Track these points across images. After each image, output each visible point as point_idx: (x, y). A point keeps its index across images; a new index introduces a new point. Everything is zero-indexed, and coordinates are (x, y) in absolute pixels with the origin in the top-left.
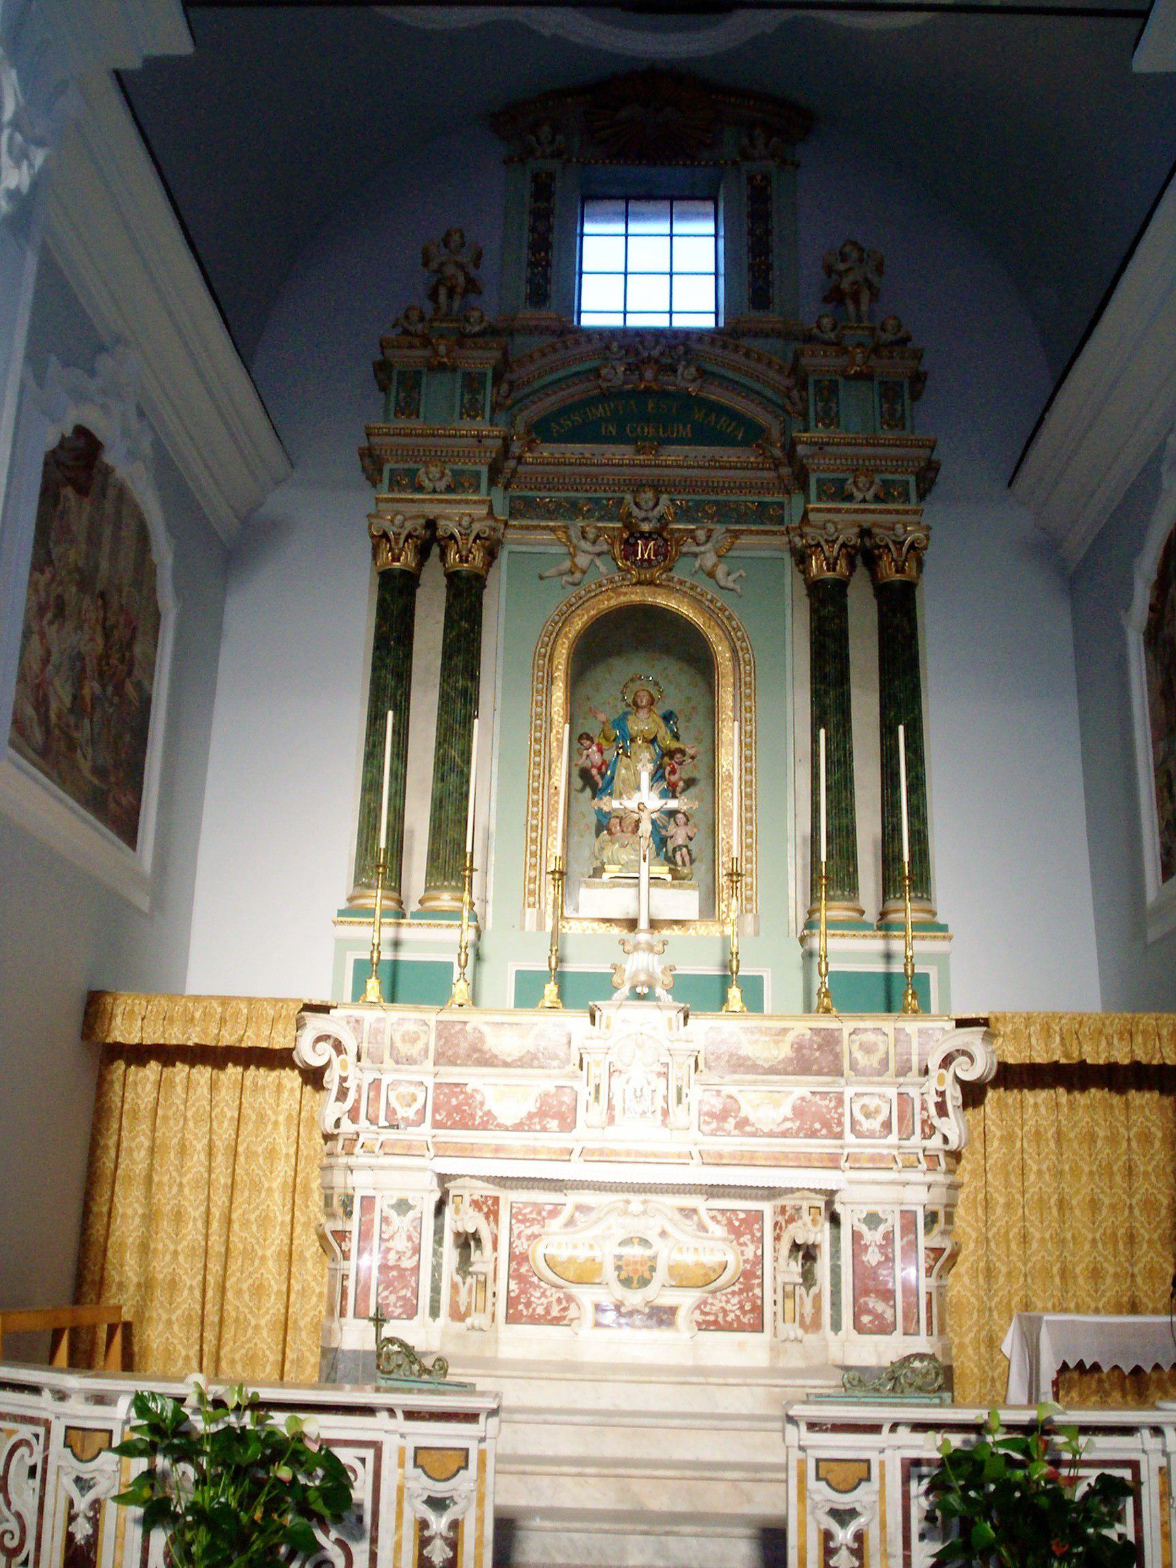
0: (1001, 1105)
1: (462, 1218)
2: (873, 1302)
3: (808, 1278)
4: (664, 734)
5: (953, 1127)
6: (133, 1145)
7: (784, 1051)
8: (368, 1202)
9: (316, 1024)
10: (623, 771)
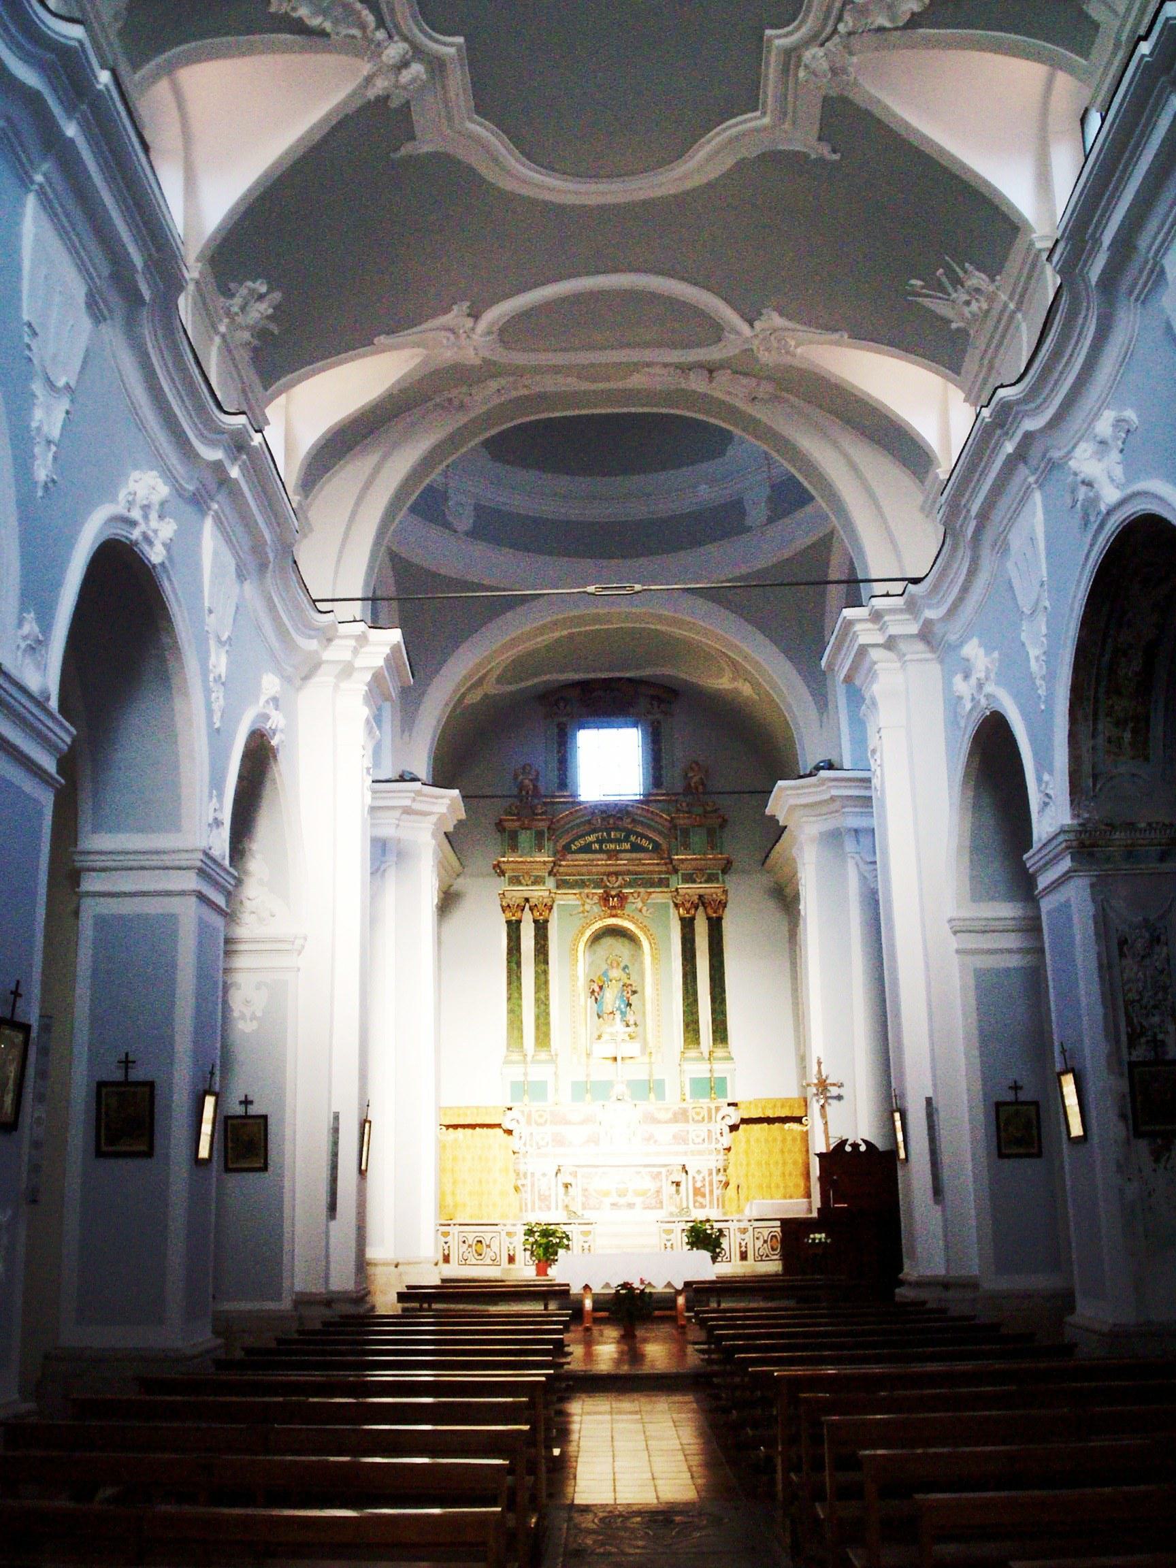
0: (745, 1131)
1: (565, 1178)
2: (700, 1199)
3: (678, 1191)
4: (624, 977)
5: (727, 1139)
7: (670, 1115)
8: (532, 1174)
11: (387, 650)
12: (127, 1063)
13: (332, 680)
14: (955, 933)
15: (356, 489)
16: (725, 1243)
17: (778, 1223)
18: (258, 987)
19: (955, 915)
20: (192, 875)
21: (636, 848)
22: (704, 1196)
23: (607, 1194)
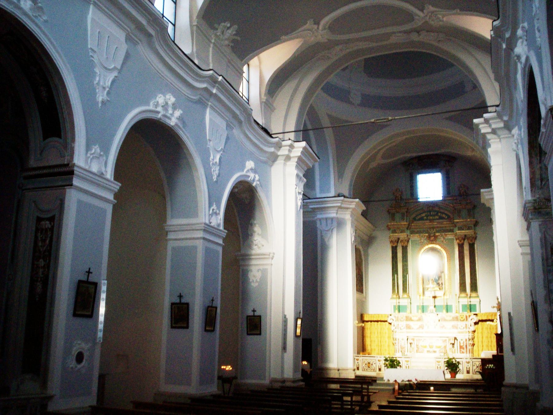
2: (462, 350)
3: (453, 347)
5: (473, 328)
6: (442, 354)
7: (451, 318)
9: (390, 317)
10: (539, 39)
11: (301, 149)
12: (180, 296)
13: (283, 161)
14: (521, 246)
15: (291, 92)
16: (460, 366)
17: (480, 360)
18: (258, 270)
19: (520, 239)
20: (202, 232)
21: (441, 218)
22: (464, 349)
23: (425, 347)
